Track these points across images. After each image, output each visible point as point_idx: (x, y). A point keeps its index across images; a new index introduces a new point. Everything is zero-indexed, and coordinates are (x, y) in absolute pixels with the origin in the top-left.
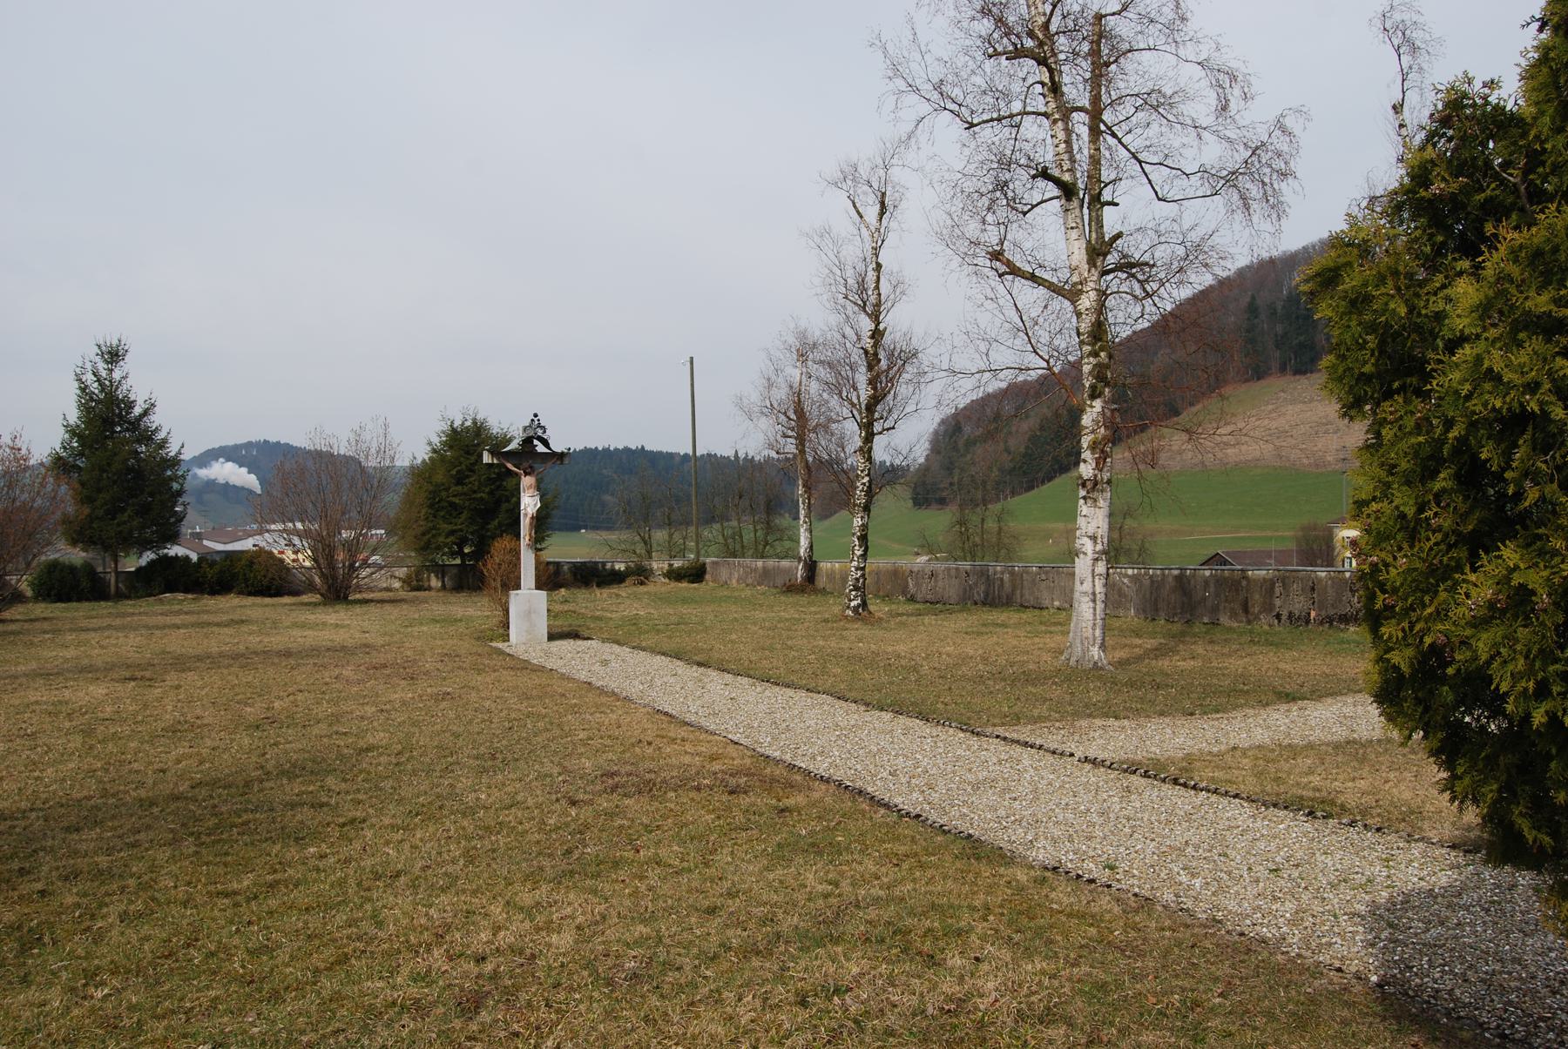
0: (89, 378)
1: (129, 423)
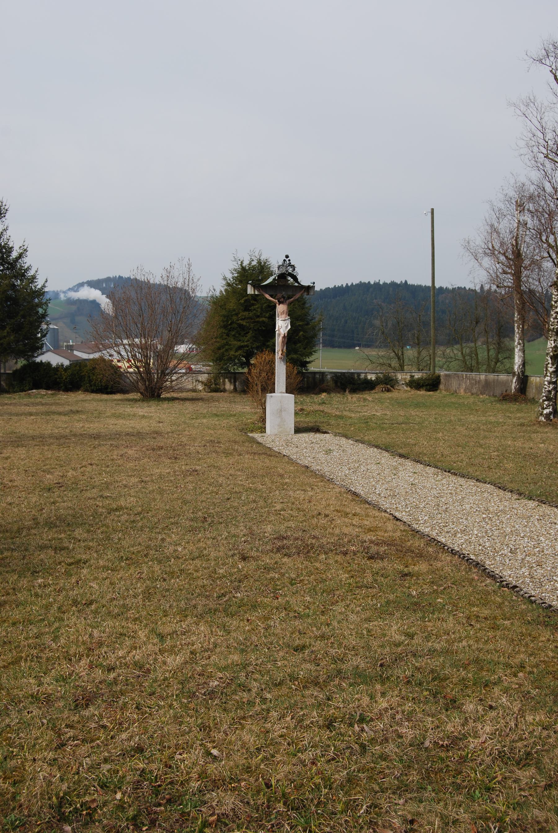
1: (9, 263)
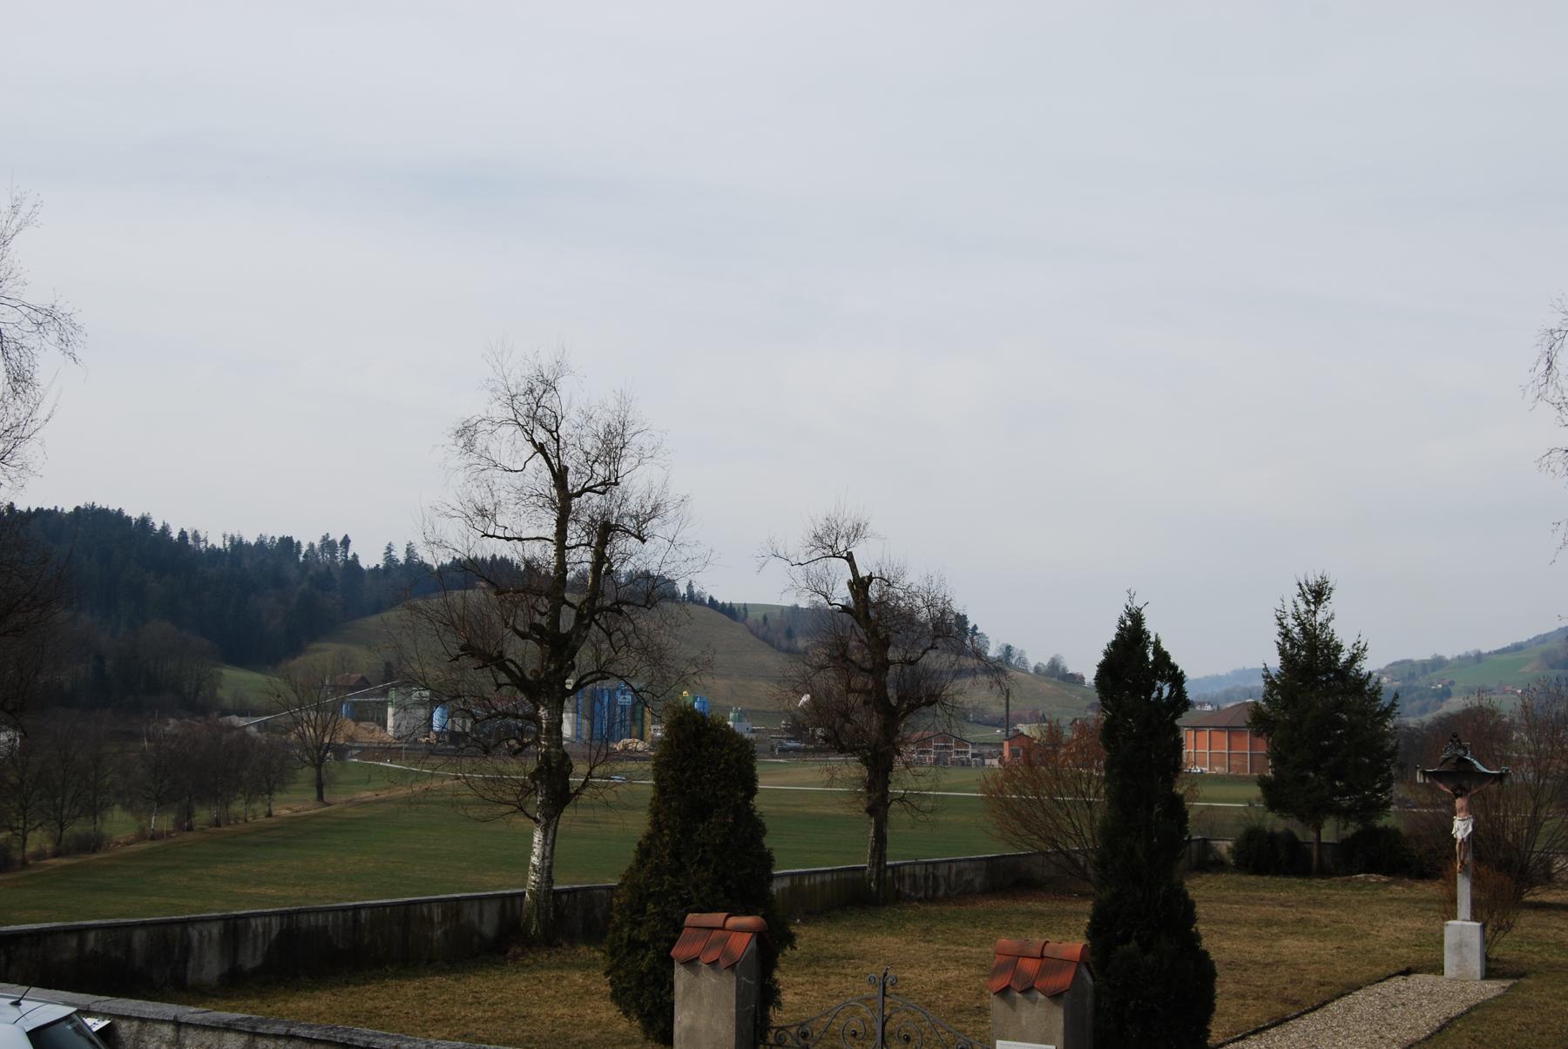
0: (1290, 622)
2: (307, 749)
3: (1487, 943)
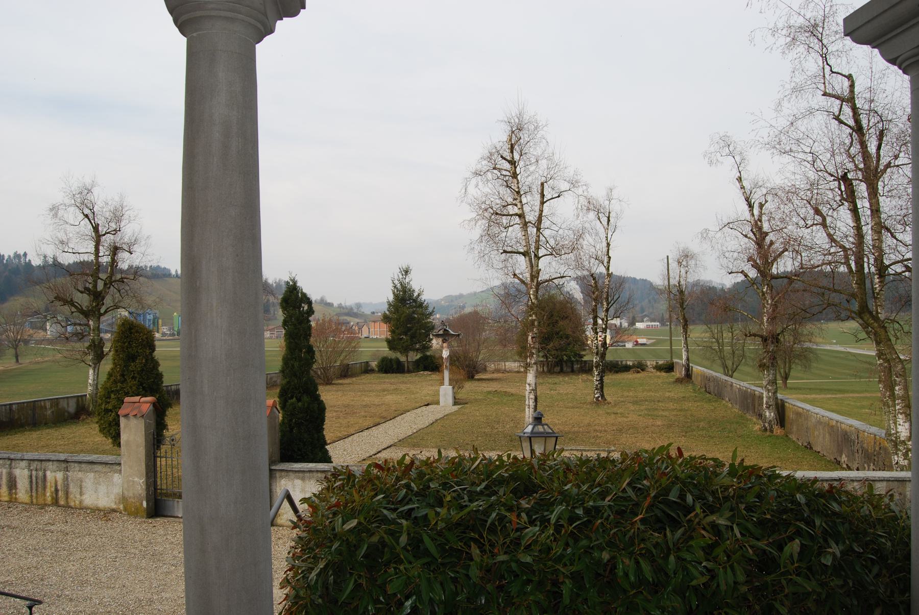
0: (396, 282)
2: (10, 341)
3: (454, 393)
